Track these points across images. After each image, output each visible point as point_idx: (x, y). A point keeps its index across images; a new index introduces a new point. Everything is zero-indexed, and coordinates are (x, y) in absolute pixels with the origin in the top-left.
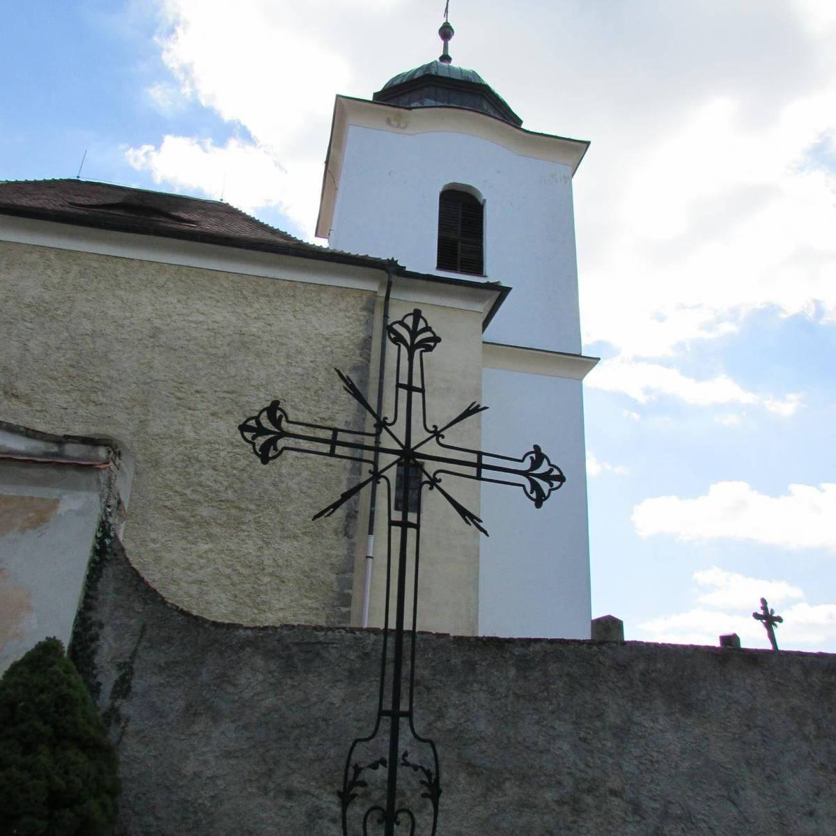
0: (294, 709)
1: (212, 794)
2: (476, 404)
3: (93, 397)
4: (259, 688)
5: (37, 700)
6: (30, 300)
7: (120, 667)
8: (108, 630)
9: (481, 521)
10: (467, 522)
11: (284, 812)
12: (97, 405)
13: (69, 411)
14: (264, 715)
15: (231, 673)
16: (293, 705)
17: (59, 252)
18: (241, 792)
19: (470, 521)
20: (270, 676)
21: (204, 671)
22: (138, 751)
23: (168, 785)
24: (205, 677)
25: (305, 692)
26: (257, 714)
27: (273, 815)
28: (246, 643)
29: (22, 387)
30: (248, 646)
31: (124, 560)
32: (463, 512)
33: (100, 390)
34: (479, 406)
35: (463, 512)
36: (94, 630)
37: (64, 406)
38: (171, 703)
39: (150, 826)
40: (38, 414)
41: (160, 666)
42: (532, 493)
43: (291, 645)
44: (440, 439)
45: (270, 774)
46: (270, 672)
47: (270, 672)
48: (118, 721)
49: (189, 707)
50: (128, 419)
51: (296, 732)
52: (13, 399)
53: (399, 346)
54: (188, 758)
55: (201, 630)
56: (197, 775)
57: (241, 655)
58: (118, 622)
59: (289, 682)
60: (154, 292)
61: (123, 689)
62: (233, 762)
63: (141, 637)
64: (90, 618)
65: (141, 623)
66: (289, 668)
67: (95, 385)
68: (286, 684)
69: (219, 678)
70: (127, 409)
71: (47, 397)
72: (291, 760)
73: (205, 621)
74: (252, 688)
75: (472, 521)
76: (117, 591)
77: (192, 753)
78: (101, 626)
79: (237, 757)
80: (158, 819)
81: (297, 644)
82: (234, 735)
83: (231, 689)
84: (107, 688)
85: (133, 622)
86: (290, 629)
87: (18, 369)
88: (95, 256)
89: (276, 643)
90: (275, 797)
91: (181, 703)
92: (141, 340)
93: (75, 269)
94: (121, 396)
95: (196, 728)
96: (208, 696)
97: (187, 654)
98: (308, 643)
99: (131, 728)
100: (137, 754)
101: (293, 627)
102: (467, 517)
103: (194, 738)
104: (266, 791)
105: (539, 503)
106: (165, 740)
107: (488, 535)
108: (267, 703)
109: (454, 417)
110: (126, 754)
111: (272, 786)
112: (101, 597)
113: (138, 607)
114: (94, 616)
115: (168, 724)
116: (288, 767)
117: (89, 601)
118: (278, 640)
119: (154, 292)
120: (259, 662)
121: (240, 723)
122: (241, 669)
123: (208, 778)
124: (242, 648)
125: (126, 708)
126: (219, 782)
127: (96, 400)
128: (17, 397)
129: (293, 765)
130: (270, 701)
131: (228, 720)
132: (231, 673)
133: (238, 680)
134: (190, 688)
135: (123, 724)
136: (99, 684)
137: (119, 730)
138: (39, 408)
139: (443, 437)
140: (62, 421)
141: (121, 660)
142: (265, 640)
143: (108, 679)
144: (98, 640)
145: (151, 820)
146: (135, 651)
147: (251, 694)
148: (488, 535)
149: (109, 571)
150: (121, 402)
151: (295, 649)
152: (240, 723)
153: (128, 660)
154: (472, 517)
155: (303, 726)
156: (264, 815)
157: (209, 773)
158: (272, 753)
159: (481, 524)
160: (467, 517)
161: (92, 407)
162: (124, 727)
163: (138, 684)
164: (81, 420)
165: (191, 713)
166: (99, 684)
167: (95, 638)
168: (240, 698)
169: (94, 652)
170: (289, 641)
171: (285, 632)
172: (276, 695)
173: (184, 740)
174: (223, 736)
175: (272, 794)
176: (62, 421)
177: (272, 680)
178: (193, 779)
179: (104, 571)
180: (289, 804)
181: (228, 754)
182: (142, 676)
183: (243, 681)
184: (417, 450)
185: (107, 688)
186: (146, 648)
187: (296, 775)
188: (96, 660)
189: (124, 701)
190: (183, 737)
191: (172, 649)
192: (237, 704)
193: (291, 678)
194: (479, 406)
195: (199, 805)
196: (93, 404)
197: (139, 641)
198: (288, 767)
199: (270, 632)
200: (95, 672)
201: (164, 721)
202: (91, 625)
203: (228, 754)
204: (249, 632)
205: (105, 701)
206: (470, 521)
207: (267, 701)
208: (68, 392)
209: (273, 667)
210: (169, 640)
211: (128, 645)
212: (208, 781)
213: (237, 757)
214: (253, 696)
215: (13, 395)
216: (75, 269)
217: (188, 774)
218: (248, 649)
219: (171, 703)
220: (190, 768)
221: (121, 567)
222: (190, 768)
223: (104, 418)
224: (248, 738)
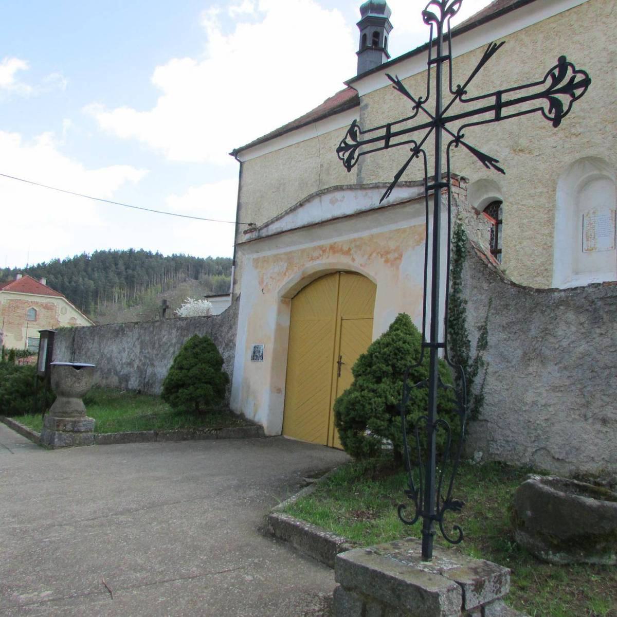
0: (603, 353)
1: (546, 417)
2: (493, 44)
3: (573, 131)
4: (573, 338)
5: (382, 351)
6: (516, 76)
7: (480, 328)
8: (470, 305)
9: (497, 161)
10: (488, 167)
11: (601, 435)
12: (577, 136)
13: (559, 147)
14: (580, 359)
15: (551, 327)
16: (602, 350)
17: (526, 30)
18: (566, 417)
19: (488, 164)
20: (581, 327)
21: (532, 327)
22: (496, 386)
23: (516, 409)
24: (533, 332)
25: (612, 339)
26: (573, 359)
27: (592, 437)
28: (561, 302)
29: (523, 142)
30: (562, 305)
31: (474, 254)
32: (483, 158)
33: (576, 123)
34: (495, 44)
35: (483, 158)
36: (463, 305)
37: (554, 145)
38: (513, 352)
39: (508, 436)
40: (538, 158)
41: (503, 327)
42: (550, 112)
43: (596, 300)
44: (422, 100)
45: (587, 405)
46: (581, 324)
47: (581, 324)
48: (482, 364)
49: (525, 354)
50: (603, 138)
51: (607, 372)
52: (521, 154)
53: (432, 25)
54: (527, 391)
55: (528, 296)
56: (534, 403)
57: (557, 312)
58: (475, 298)
59: (598, 331)
60: (604, 23)
61: (483, 344)
62: (560, 394)
63: (489, 307)
64: (459, 298)
65: (489, 297)
66: (596, 320)
67: (573, 121)
68: (595, 333)
69: (543, 331)
70: (600, 130)
71: (542, 143)
72: (604, 395)
73: (531, 289)
74: (568, 338)
75: (491, 163)
76: (473, 277)
77: (530, 388)
78: (466, 302)
79: (562, 391)
80: (513, 432)
81: (601, 299)
82: (559, 375)
83: (552, 340)
84: (474, 343)
85: (483, 297)
86: (596, 287)
87: (518, 131)
88: (552, 19)
89: (583, 300)
90: (593, 424)
91: (519, 352)
92: (601, 69)
93: (541, 36)
94: (594, 122)
95: (531, 369)
96: (537, 346)
97: (520, 316)
98: (611, 297)
99: (490, 370)
100: (495, 388)
101: (599, 284)
102: (486, 162)
103: (530, 376)
104: (586, 418)
105: (556, 122)
106: (512, 378)
107: (504, 173)
108: (581, 349)
109: (477, 64)
110: (489, 387)
111: (590, 414)
112: (463, 283)
113: (485, 286)
114: (462, 296)
115: (513, 367)
116: (602, 400)
117: (457, 287)
118: (585, 298)
119: (604, 23)
120: (571, 316)
121: (561, 365)
122: (558, 323)
123: (542, 406)
124: (557, 307)
125: (486, 356)
126: (550, 409)
127: (576, 132)
128: (521, 150)
129: (605, 398)
130: (583, 347)
131: (552, 363)
132: (551, 327)
133: (556, 332)
134: (524, 341)
135: (485, 368)
136: (469, 341)
137: (484, 371)
138: (538, 154)
139: (421, 98)
140: (555, 157)
141: (479, 325)
142: (575, 298)
143: (473, 337)
144: (465, 312)
145: (508, 432)
146: (487, 317)
147: (568, 343)
148: (504, 173)
149: (467, 265)
150: (595, 126)
151: (600, 303)
152: (561, 365)
153: (484, 324)
154: (491, 160)
155: (611, 367)
156: (585, 437)
157: (543, 402)
158: (588, 389)
159: (497, 164)
160: (486, 162)
161: (574, 139)
162: (486, 370)
163: (492, 339)
164: (568, 151)
165: (526, 359)
166: (469, 341)
167: (464, 310)
168: (560, 346)
169: (464, 321)
170: (594, 297)
171: (591, 290)
172: (588, 342)
173: (523, 378)
174: (550, 375)
175: (590, 421)
176: (555, 157)
177: (583, 330)
178: (532, 406)
179: (463, 265)
180: (605, 430)
181: (555, 389)
182: (493, 334)
183: (560, 333)
184: (434, 115)
185: (474, 343)
186: (493, 314)
187: (609, 407)
188: (466, 326)
189: (484, 351)
190: (523, 376)
191: (510, 313)
192: (558, 351)
193: (598, 327)
194: (495, 44)
195: (538, 425)
196: (574, 136)
197: (489, 310)
198: (602, 400)
199: (579, 291)
200: (466, 333)
201: (510, 365)
202: (461, 302)
203: (555, 389)
204: (563, 294)
205: (473, 353)
206: (488, 164)
207: (581, 348)
208: (554, 134)
209: (583, 320)
210: (507, 306)
211: (482, 313)
212: (543, 408)
213: (562, 391)
214: (569, 344)
215: (520, 150)
216: (541, 36)
217: (528, 402)
218: (562, 307)
219: (513, 352)
220: (529, 397)
221: (473, 260)
222: (529, 397)
223: (584, 144)
224: (568, 377)
